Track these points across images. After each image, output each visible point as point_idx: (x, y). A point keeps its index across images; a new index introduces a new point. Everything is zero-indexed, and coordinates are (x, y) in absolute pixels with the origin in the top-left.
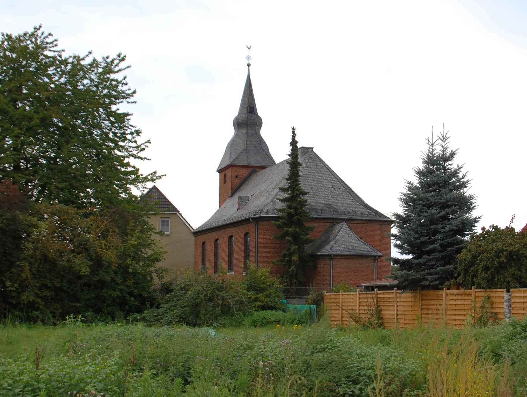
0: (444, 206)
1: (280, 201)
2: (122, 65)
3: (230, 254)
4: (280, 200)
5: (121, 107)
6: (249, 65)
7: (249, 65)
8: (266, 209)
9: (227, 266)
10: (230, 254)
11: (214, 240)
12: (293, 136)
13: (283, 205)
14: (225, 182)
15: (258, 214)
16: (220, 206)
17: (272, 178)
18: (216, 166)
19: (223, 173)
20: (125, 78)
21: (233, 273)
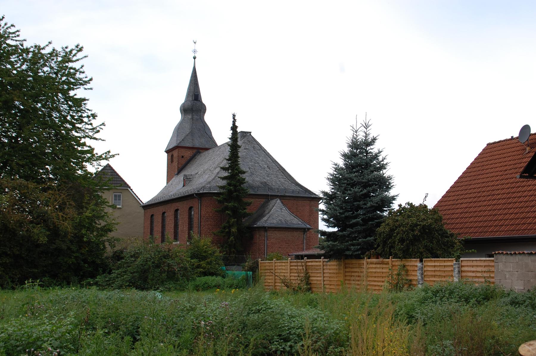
5: (78, 93)
6: (195, 58)
7: (195, 58)
13: (224, 183)
16: (167, 183)
19: (171, 154)
20: (82, 66)
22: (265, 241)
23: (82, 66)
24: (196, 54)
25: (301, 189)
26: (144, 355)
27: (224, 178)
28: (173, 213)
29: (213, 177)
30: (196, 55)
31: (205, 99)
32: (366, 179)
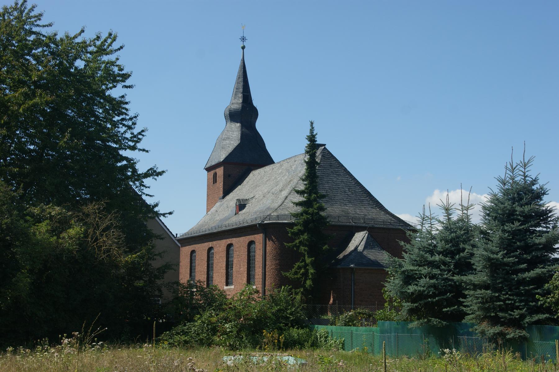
0: (527, 218)
1: (294, 204)
2: (115, 46)
3: (229, 266)
4: (294, 203)
5: (116, 93)
6: (243, 48)
7: (243, 48)
8: (275, 214)
9: (224, 280)
10: (229, 266)
11: (207, 249)
12: (311, 130)
13: (299, 209)
14: (215, 181)
15: (266, 219)
16: (208, 210)
17: (276, 178)
18: (203, 163)
19: (212, 172)
20: (117, 59)
21: (233, 287)
22: (352, 286)
23: (117, 59)
24: (244, 42)
25: (393, 219)
26: (484, 371)
27: (297, 204)
28: (225, 248)
29: (280, 202)
30: (245, 44)
31: (256, 103)
32: (224, 227)
